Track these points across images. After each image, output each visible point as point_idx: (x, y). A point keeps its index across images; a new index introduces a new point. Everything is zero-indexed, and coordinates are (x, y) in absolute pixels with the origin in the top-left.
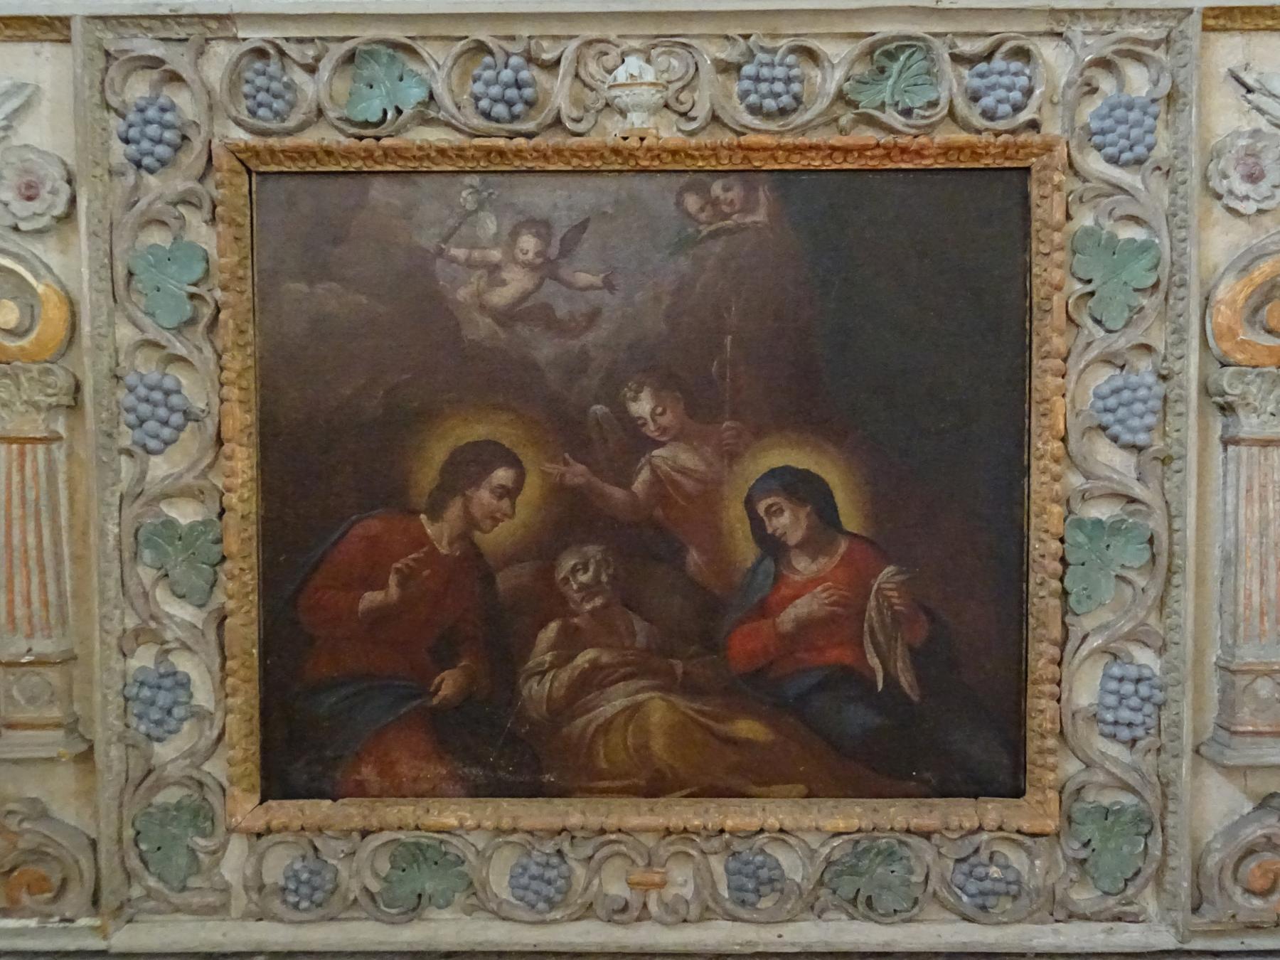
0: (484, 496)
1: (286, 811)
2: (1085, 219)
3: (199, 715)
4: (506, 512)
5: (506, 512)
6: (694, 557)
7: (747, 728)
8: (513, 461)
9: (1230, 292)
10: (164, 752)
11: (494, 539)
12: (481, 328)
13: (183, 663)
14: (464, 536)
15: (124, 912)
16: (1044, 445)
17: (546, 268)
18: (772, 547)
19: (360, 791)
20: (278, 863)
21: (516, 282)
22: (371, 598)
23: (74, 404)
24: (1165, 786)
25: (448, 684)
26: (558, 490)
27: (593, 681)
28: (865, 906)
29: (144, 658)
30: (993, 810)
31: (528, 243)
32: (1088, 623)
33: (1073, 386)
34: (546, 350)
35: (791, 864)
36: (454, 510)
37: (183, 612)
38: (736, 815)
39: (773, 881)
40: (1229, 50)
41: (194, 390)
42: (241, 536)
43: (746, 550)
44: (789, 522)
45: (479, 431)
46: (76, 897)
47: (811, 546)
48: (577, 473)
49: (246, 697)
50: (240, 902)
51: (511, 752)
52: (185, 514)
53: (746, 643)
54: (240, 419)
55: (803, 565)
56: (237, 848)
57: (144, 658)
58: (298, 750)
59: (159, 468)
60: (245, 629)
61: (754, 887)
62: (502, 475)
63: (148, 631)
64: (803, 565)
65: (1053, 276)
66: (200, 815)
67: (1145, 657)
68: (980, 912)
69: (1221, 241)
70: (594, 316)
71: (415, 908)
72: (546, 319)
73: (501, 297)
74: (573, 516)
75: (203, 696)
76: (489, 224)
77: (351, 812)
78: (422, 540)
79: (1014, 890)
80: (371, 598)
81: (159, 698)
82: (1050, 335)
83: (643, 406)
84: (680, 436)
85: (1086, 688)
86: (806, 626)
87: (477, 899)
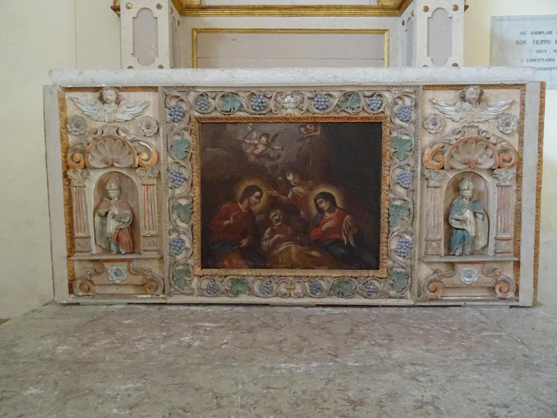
0: (253, 198)
1: (207, 271)
2: (395, 134)
3: (187, 249)
4: (258, 202)
5: (258, 202)
6: (302, 213)
7: (315, 253)
8: (260, 190)
9: (428, 152)
10: (178, 257)
11: (257, 208)
12: (252, 159)
13: (183, 237)
14: (248, 208)
15: (170, 294)
16: (384, 187)
17: (268, 145)
18: (321, 211)
19: (224, 267)
20: (205, 283)
21: (261, 148)
22: (227, 222)
23: (159, 177)
24: (412, 267)
25: (244, 242)
26: (270, 197)
27: (279, 242)
28: (341, 295)
29: (174, 236)
30: (372, 273)
31: (264, 139)
32: (395, 229)
33: (391, 173)
34: (268, 164)
35: (324, 285)
36: (246, 202)
37: (183, 225)
38: (311, 273)
39: (320, 289)
40: (430, 94)
41: (186, 173)
42: (197, 207)
43: (315, 212)
44: (324, 205)
45: (252, 183)
46: (160, 290)
47: (329, 211)
48: (275, 193)
49: (198, 245)
50: (196, 292)
51: (259, 258)
52: (184, 202)
53: (314, 234)
54: (197, 180)
55: (328, 215)
56: (196, 280)
57: (174, 236)
58: (209, 258)
59: (178, 191)
60: (198, 228)
61: (316, 290)
62: (257, 194)
63: (176, 229)
64: (328, 215)
65: (387, 148)
66: (187, 272)
67: (408, 237)
68: (368, 296)
69: (427, 139)
70: (279, 156)
71: (237, 294)
72: (268, 156)
73: (257, 152)
74: (273, 203)
75: (188, 244)
76: (255, 135)
77: (222, 272)
78: (238, 208)
79: (376, 291)
80: (227, 222)
81: (177, 245)
82: (386, 161)
83: (290, 178)
84: (299, 185)
85: (394, 244)
86: (328, 229)
87: (251, 292)
